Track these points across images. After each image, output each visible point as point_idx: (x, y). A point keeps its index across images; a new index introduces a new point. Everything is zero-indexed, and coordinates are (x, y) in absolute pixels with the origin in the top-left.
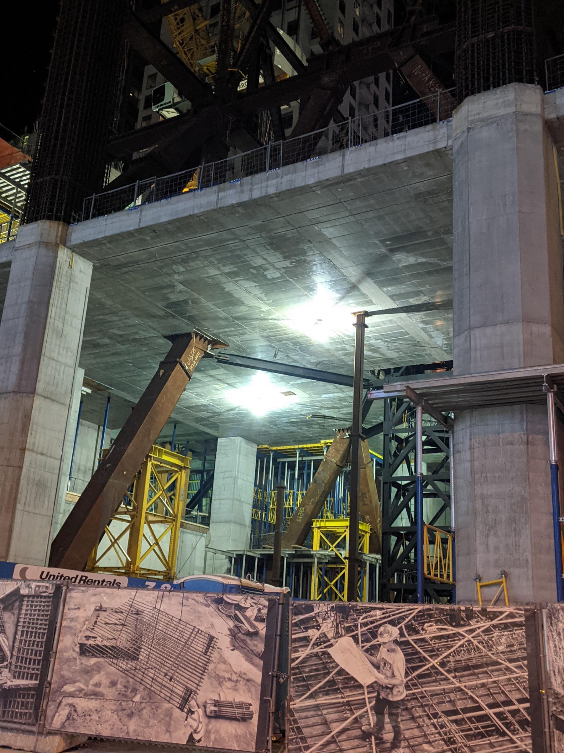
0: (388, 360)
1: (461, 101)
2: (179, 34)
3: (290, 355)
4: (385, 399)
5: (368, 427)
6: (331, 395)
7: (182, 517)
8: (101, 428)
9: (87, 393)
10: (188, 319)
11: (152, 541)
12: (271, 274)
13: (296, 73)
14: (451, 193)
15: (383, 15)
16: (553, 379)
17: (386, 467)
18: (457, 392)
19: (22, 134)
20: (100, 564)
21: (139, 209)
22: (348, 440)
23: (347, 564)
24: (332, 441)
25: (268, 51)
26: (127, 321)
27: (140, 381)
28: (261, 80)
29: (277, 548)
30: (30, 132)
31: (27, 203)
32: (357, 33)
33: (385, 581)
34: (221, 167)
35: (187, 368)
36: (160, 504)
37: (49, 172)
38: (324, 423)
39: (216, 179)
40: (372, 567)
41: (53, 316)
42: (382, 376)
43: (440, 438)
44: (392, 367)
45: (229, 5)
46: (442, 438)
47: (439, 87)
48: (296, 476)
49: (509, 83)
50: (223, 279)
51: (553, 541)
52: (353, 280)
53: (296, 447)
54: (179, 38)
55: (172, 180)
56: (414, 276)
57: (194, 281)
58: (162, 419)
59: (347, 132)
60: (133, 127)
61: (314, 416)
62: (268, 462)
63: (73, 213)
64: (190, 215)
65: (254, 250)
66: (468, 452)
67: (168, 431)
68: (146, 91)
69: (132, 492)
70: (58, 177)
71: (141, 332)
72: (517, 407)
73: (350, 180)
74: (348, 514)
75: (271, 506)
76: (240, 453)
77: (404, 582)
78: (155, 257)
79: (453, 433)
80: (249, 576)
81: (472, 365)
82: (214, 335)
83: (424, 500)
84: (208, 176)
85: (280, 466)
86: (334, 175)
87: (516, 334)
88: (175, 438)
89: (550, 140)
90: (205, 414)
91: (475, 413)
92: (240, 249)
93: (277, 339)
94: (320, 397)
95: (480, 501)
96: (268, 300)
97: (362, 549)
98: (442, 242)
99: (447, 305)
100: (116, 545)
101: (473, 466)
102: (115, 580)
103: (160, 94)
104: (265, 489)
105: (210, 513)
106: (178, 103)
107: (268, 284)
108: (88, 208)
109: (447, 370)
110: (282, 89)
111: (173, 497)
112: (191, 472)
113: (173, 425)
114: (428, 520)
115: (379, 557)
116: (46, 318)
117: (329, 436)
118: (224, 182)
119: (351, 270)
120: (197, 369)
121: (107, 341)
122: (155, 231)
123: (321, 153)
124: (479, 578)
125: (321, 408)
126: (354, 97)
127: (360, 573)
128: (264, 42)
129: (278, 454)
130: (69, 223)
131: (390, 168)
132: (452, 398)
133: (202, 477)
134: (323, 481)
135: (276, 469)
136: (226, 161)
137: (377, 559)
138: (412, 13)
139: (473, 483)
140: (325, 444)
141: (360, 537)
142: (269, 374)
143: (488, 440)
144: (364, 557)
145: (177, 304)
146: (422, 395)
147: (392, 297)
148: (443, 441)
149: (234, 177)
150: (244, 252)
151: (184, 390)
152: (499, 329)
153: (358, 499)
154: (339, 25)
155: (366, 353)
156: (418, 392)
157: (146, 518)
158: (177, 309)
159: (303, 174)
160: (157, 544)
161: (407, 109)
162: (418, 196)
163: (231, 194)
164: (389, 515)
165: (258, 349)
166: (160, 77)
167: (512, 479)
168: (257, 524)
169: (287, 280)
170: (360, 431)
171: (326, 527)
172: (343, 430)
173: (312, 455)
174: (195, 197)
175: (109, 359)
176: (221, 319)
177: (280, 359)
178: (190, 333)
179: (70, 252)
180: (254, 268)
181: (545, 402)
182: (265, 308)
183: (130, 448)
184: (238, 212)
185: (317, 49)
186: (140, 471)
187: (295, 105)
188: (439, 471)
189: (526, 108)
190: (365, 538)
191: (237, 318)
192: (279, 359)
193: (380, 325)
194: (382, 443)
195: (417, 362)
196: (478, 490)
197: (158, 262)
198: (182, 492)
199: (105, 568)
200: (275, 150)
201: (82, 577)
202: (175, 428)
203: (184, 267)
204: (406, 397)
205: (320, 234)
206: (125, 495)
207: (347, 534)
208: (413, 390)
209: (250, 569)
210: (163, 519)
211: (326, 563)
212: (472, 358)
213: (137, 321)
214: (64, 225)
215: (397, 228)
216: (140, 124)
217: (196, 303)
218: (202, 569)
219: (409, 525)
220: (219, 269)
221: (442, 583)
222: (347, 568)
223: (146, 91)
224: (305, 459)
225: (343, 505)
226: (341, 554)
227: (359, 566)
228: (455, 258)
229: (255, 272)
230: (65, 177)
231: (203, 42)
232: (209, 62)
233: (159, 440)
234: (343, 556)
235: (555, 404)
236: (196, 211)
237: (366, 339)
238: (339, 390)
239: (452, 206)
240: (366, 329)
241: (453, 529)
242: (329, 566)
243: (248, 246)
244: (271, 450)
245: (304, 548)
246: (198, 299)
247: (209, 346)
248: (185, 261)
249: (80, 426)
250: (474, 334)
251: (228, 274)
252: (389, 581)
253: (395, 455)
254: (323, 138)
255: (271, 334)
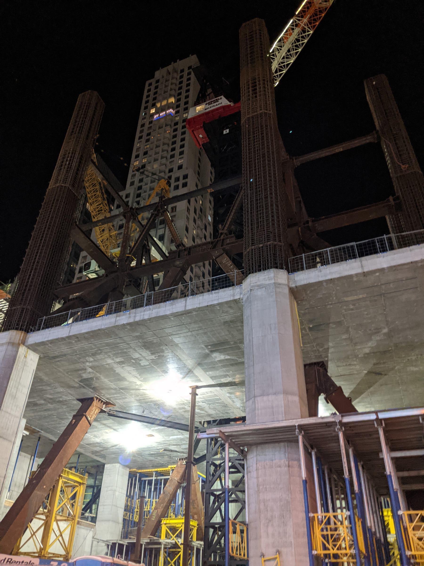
0: (209, 415)
1: (247, 276)
2: (101, 237)
3: (152, 411)
4: (208, 438)
5: (197, 457)
6: (175, 437)
7: (79, 517)
8: (33, 457)
9: (26, 435)
10: (92, 389)
11: (58, 533)
12: (144, 363)
13: (162, 259)
14: (242, 322)
15: (208, 234)
16: (301, 427)
17: (207, 483)
18: (249, 434)
19: (6, 283)
20: (22, 550)
21: (70, 325)
22: (185, 466)
23: (182, 549)
24: (175, 466)
25: (148, 247)
26: (56, 390)
27: (59, 427)
28: (144, 262)
29: (138, 539)
30: (12, 282)
31: (5, 320)
32: (194, 242)
33: (206, 559)
34: (119, 304)
35: (89, 419)
36: (65, 508)
37: (20, 303)
38: (171, 455)
39: (115, 310)
40: (198, 550)
41: (11, 386)
42: (206, 425)
43: (239, 464)
44: (212, 419)
45: (129, 225)
46: (240, 464)
47: (236, 269)
48: (153, 490)
49: (271, 268)
50: (115, 366)
51: (306, 529)
52: (190, 367)
53: (153, 470)
54: (101, 239)
55: (90, 310)
56: (224, 366)
57: (98, 366)
58: (71, 451)
59: (188, 289)
60: (71, 282)
61: (165, 450)
62: (136, 480)
63: (31, 327)
64: (99, 329)
65: (135, 350)
66: (255, 472)
67: (74, 459)
68: (81, 264)
69: (48, 500)
70: (25, 307)
71: (64, 397)
72: (282, 444)
73: (189, 313)
74: (184, 515)
75: (136, 510)
76: (118, 475)
77: (218, 560)
78: (76, 352)
79: (246, 460)
80: (119, 557)
81: (257, 418)
82: (107, 399)
83: (230, 504)
84: (111, 308)
85: (143, 483)
86: (181, 310)
87: (279, 401)
88: (78, 464)
89: (293, 298)
90: (98, 449)
91: (259, 448)
92: (126, 349)
93: (144, 402)
94: (169, 438)
95: (263, 503)
96: (141, 378)
97: (192, 538)
98: (239, 348)
99: (242, 383)
100: (34, 536)
101: (258, 481)
102: (30, 561)
103: (88, 266)
104: (133, 499)
105: (97, 514)
106: (98, 271)
107: (142, 369)
108: (40, 324)
109: (243, 422)
110: (155, 266)
111: (74, 504)
112: (87, 487)
113: (77, 456)
114: (232, 517)
115: (202, 543)
116: (7, 387)
117: (174, 463)
118: (120, 311)
119: (189, 361)
120: (96, 420)
121: (43, 402)
122: (78, 337)
123: (174, 299)
124: (263, 555)
125: (170, 445)
126: (192, 273)
127: (190, 554)
128: (146, 243)
129: (142, 475)
130: (28, 332)
131: (210, 308)
132: (245, 438)
133: (93, 491)
134: (169, 493)
135: (140, 484)
136: (122, 301)
137: (201, 545)
138: (222, 234)
139: (258, 492)
140: (171, 468)
141: (191, 530)
142: (139, 423)
143: (267, 465)
144: (193, 543)
145: (87, 380)
146: (228, 436)
147: (212, 378)
148: (241, 466)
149: (126, 309)
150: (128, 350)
151: (87, 433)
152: (271, 397)
153: (190, 504)
154: (185, 238)
155: (197, 411)
156: (226, 434)
157: (55, 517)
158: (87, 383)
159: (164, 309)
160: (61, 535)
161: (219, 279)
162: (225, 322)
163: (124, 318)
164: (209, 515)
165: (134, 408)
166: (89, 257)
167: (281, 489)
168: (127, 522)
169: (153, 367)
170: (192, 460)
171: (169, 524)
172: (182, 459)
173: (163, 475)
174: (103, 320)
175: (42, 413)
176: (112, 389)
177: (146, 414)
178: (93, 398)
179: (26, 348)
180: (134, 359)
181: (297, 441)
182: (139, 383)
183: (50, 470)
184: (127, 328)
185: (174, 248)
186: (54, 486)
187: (161, 274)
188: (239, 485)
189: (280, 281)
190: (194, 531)
191: (122, 389)
192: (145, 414)
193: (205, 394)
194: (205, 468)
195: (226, 417)
196: (262, 496)
197: (78, 355)
198: (80, 500)
199: (25, 553)
200: (149, 297)
201: (9, 559)
202: (79, 458)
203: (93, 358)
204: (220, 437)
205: (172, 341)
206: (43, 502)
207: (183, 528)
208: (223, 433)
209: (120, 552)
210: (66, 518)
211: (170, 548)
212: (257, 414)
213: (61, 390)
214: (24, 333)
215: (214, 340)
216: (75, 281)
217: (98, 379)
218: (90, 553)
219: (221, 521)
220: (113, 359)
221: (241, 560)
222: (182, 551)
223: (81, 264)
224: (159, 478)
225: (181, 509)
226: (179, 542)
227: (190, 550)
228: (246, 356)
229: (134, 361)
230: (29, 307)
231: (114, 241)
232: (116, 251)
233: (67, 465)
234: (180, 543)
235: (303, 442)
236: (103, 327)
237: (197, 402)
238: (180, 434)
239: (243, 329)
240: (197, 396)
241: (247, 523)
242: (171, 550)
243: (131, 347)
244: (137, 472)
245: (155, 538)
246: (100, 377)
247: (104, 406)
248: (94, 355)
249: (19, 456)
250: (257, 400)
251: (119, 363)
252: (208, 559)
253: (213, 475)
254: (175, 291)
255: (141, 398)
